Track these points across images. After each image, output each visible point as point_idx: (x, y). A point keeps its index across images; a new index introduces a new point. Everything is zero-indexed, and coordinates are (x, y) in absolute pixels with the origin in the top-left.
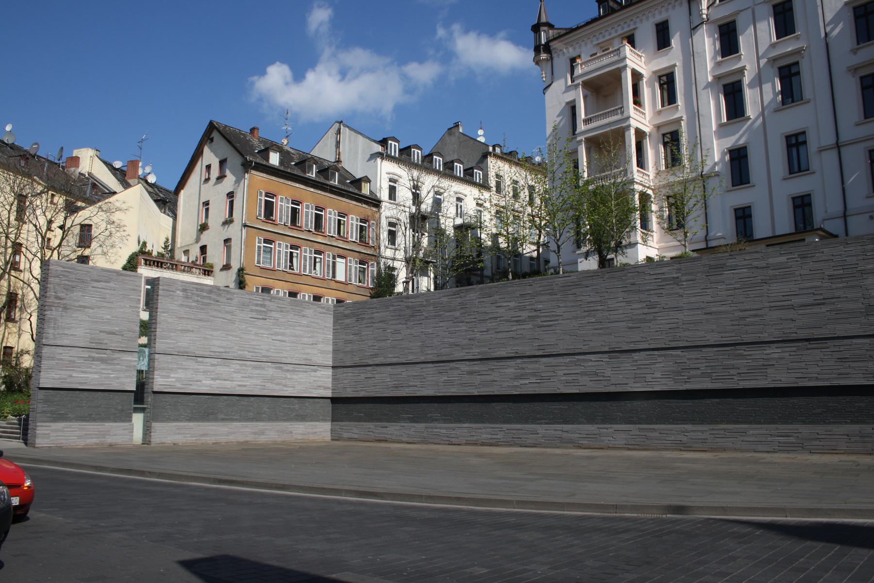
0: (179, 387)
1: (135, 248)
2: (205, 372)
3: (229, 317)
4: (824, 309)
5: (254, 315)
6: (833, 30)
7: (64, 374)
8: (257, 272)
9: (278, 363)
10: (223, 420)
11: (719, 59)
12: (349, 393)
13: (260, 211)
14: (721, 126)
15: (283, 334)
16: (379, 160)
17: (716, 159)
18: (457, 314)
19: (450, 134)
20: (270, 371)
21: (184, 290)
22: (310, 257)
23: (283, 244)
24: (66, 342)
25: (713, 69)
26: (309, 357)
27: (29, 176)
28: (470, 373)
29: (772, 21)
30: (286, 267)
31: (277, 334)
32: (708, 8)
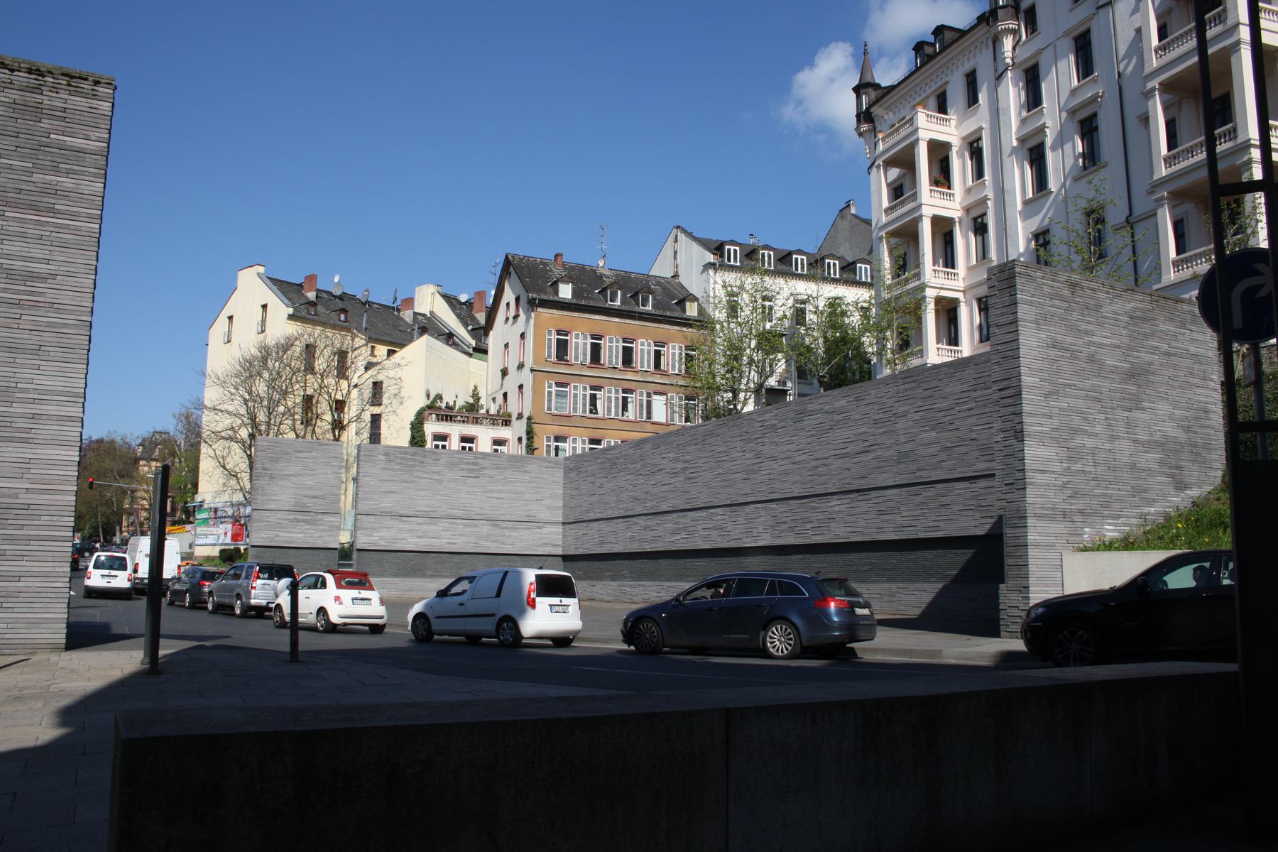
0: (382, 545)
1: (422, 402)
2: (411, 531)
3: (436, 477)
4: (870, 456)
5: (465, 473)
6: (1127, 66)
7: (271, 534)
8: (548, 420)
9: (494, 521)
10: (432, 576)
11: (1024, 114)
12: (572, 552)
13: (549, 352)
14: (1026, 203)
15: (499, 491)
16: (711, 272)
17: (1021, 250)
18: (638, 466)
19: (842, 217)
20: (485, 528)
21: (386, 454)
22: (617, 399)
23: (580, 386)
24: (273, 507)
25: (1019, 129)
26: (532, 513)
27: (348, 330)
28: (646, 528)
29: (1072, 59)
30: (584, 411)
31: (492, 491)
32: (1014, 48)
